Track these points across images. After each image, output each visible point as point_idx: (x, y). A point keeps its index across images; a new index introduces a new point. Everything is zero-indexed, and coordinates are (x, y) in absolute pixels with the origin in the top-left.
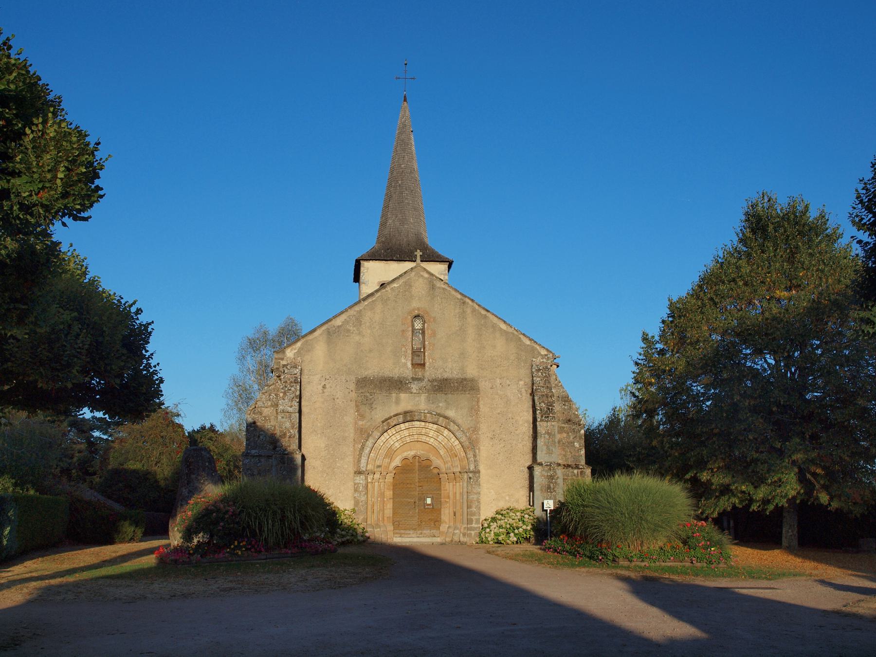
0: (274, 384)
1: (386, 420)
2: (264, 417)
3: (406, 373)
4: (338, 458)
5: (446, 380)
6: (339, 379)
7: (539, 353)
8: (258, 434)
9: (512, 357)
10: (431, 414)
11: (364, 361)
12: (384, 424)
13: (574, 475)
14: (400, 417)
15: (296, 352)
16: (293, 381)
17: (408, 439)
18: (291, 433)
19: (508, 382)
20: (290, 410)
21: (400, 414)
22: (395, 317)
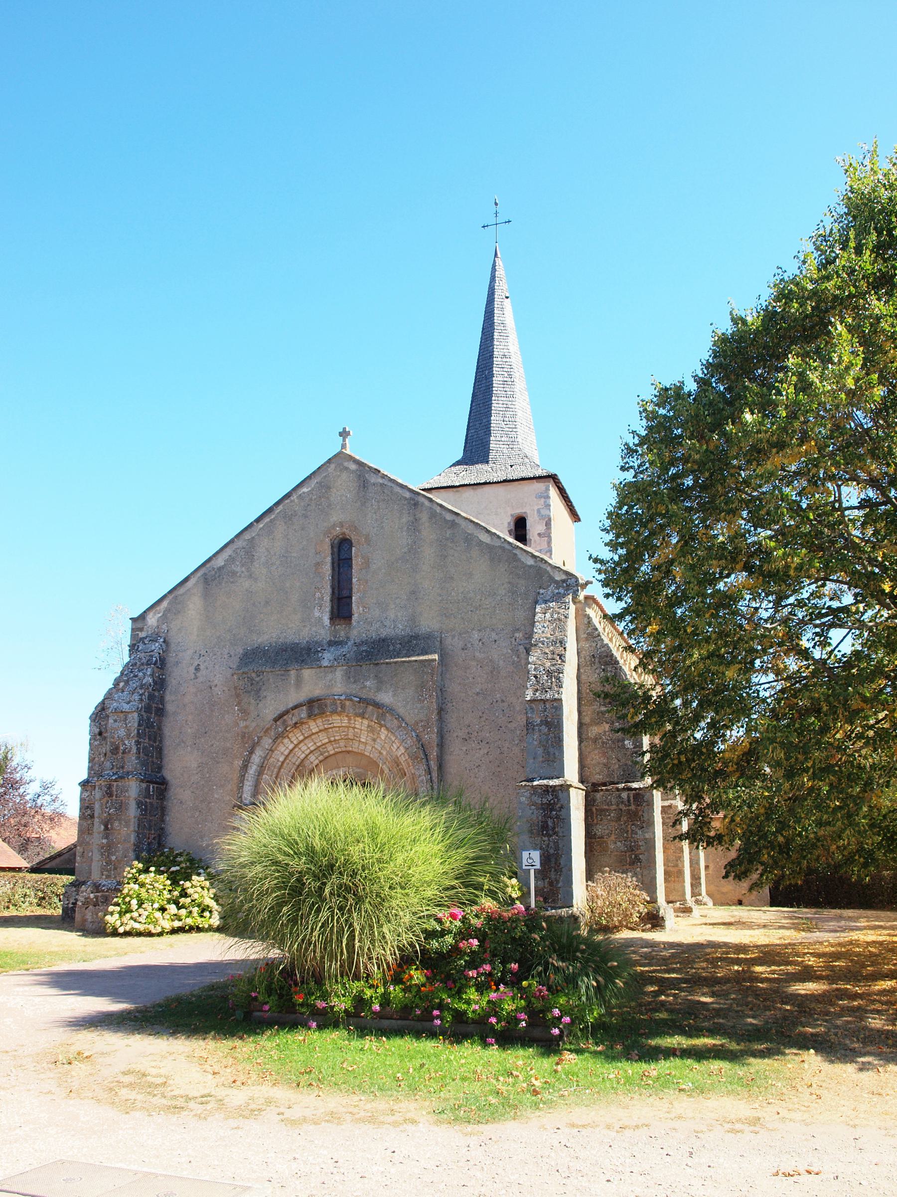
1: (280, 716)
3: (320, 634)
4: (216, 785)
5: (383, 640)
9: (502, 592)
10: (351, 700)
11: (257, 621)
12: (278, 723)
13: (622, 802)
17: (331, 750)
19: (494, 636)
20: (126, 707)
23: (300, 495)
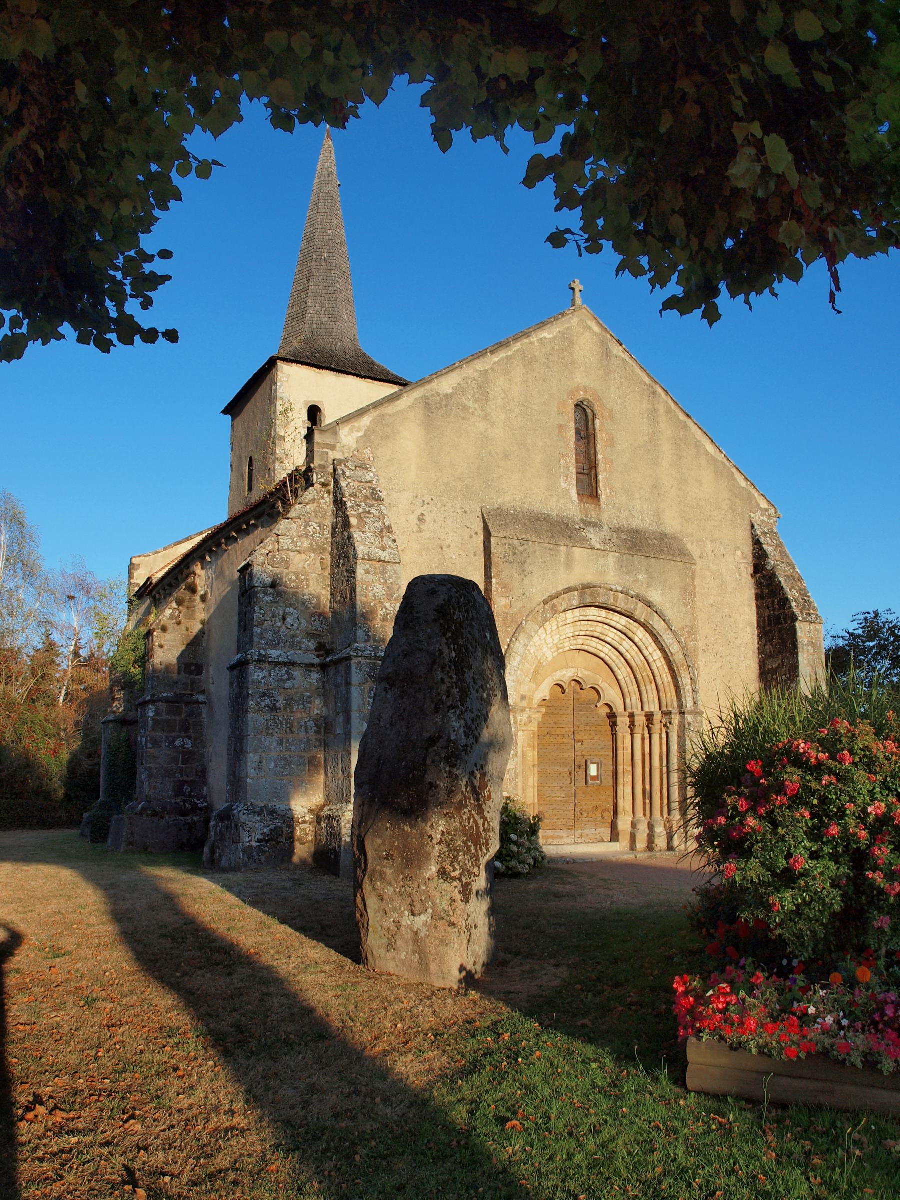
0: (314, 500)
1: (552, 598)
2: (294, 573)
3: (570, 510)
6: (449, 505)
7: (758, 505)
8: (282, 613)
10: (627, 594)
11: (495, 476)
12: (547, 607)
14: (574, 596)
16: (368, 494)
18: (387, 609)
21: (575, 589)
22: (546, 397)
23: (541, 339)
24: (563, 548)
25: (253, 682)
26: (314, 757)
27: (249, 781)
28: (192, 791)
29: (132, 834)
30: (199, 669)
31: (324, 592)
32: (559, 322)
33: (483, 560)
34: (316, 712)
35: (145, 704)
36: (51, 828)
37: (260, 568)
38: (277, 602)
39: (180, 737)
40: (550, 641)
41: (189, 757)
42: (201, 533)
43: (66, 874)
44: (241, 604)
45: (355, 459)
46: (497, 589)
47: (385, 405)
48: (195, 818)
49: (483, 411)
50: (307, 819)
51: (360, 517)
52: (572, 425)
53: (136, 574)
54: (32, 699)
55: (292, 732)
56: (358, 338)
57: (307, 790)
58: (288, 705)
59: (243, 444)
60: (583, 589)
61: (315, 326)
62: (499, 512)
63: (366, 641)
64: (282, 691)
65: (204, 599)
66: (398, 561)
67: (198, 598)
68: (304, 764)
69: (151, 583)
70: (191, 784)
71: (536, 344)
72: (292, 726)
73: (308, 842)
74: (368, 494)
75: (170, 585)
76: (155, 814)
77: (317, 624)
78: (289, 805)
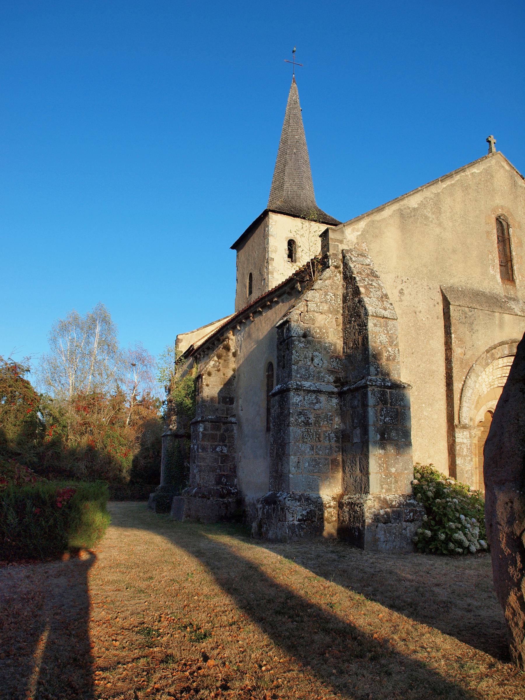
0: (330, 277)
2: (319, 327)
3: (497, 289)
6: (419, 283)
8: (311, 355)
11: (448, 264)
14: (505, 347)
15: (359, 235)
18: (389, 352)
21: (507, 343)
22: (477, 212)
23: (473, 173)
24: (497, 314)
25: (293, 404)
26: (336, 459)
27: (291, 476)
28: (227, 481)
29: (189, 509)
30: (231, 401)
31: (338, 341)
32: (483, 162)
33: (443, 322)
34: (336, 426)
35: (197, 423)
36: (122, 501)
37: (296, 324)
38: (308, 348)
39: (219, 445)
40: (486, 380)
41: (225, 458)
42: (228, 317)
43: (158, 539)
44: (279, 350)
45: (356, 250)
46: (455, 342)
47: (375, 214)
48: (230, 500)
49: (438, 220)
50: (332, 504)
51: (365, 287)
52: (495, 231)
53: (180, 345)
54: (112, 423)
55: (320, 441)
56: (315, 200)
57: (330, 482)
58: (317, 422)
59: (245, 266)
60: (511, 343)
61: (289, 193)
62: (452, 289)
63: (376, 375)
64: (312, 411)
65: (234, 354)
66: (396, 318)
67: (231, 354)
68: (328, 464)
69: (193, 349)
70: (226, 476)
71: (469, 176)
72: (319, 435)
73: (332, 522)
74: (369, 273)
75: (208, 348)
76: (203, 496)
77: (334, 364)
78: (318, 494)
